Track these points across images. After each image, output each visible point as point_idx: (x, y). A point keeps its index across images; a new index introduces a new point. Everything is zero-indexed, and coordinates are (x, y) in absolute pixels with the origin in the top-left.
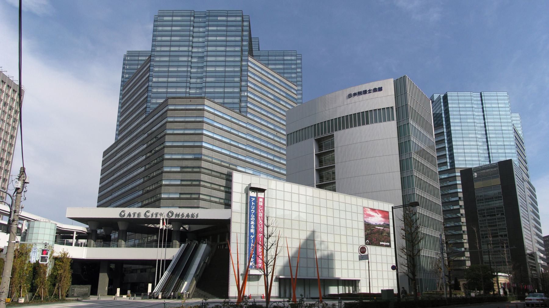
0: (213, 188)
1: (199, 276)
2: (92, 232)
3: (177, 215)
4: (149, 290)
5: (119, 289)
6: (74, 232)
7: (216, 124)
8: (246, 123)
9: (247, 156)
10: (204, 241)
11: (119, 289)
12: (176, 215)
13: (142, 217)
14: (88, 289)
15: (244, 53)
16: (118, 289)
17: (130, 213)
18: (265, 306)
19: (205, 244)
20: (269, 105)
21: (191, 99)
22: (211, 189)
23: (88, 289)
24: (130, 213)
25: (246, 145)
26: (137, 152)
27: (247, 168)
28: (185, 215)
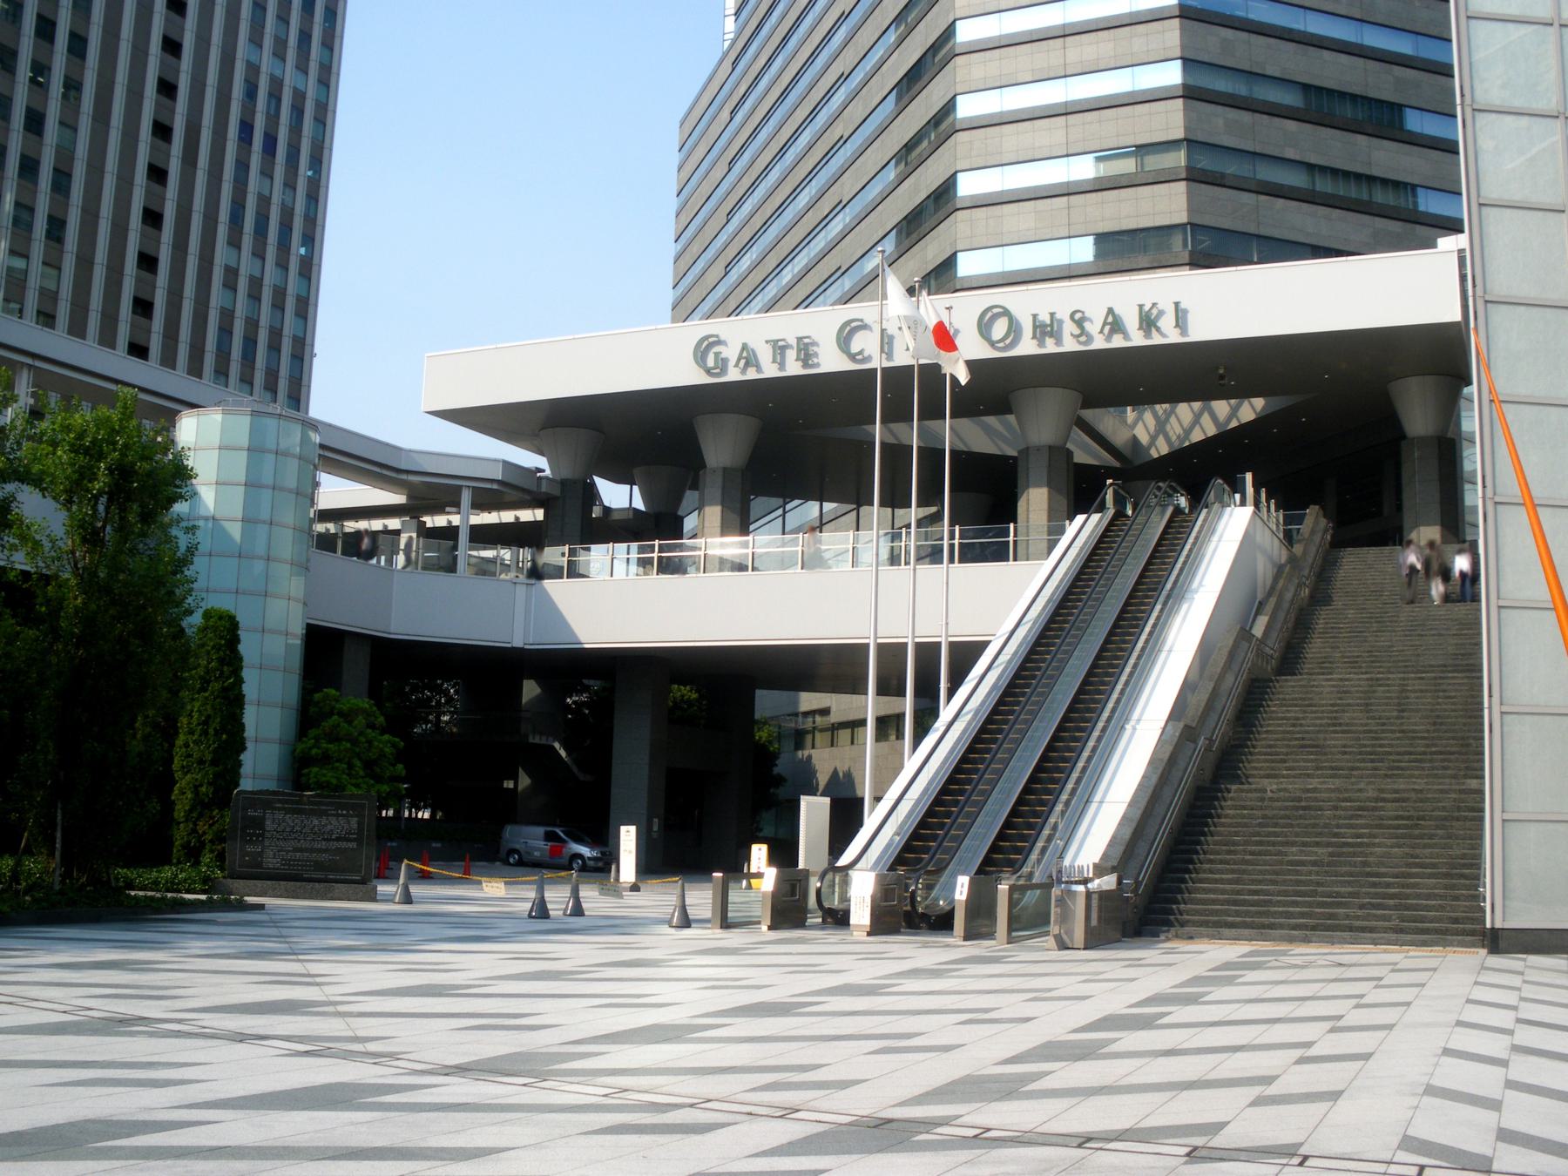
0: (1267, 183)
1: (1201, 741)
2: (563, 491)
3: (1044, 330)
4: (745, 871)
5: (633, 829)
6: (459, 489)
10: (1236, 486)
11: (633, 829)
13: (831, 361)
14: (354, 821)
16: (623, 829)
17: (1110, 311)
19: (1243, 503)
22: (1253, 196)
23: (360, 824)
24: (1110, 311)
26: (941, 1114)
28: (1131, 321)
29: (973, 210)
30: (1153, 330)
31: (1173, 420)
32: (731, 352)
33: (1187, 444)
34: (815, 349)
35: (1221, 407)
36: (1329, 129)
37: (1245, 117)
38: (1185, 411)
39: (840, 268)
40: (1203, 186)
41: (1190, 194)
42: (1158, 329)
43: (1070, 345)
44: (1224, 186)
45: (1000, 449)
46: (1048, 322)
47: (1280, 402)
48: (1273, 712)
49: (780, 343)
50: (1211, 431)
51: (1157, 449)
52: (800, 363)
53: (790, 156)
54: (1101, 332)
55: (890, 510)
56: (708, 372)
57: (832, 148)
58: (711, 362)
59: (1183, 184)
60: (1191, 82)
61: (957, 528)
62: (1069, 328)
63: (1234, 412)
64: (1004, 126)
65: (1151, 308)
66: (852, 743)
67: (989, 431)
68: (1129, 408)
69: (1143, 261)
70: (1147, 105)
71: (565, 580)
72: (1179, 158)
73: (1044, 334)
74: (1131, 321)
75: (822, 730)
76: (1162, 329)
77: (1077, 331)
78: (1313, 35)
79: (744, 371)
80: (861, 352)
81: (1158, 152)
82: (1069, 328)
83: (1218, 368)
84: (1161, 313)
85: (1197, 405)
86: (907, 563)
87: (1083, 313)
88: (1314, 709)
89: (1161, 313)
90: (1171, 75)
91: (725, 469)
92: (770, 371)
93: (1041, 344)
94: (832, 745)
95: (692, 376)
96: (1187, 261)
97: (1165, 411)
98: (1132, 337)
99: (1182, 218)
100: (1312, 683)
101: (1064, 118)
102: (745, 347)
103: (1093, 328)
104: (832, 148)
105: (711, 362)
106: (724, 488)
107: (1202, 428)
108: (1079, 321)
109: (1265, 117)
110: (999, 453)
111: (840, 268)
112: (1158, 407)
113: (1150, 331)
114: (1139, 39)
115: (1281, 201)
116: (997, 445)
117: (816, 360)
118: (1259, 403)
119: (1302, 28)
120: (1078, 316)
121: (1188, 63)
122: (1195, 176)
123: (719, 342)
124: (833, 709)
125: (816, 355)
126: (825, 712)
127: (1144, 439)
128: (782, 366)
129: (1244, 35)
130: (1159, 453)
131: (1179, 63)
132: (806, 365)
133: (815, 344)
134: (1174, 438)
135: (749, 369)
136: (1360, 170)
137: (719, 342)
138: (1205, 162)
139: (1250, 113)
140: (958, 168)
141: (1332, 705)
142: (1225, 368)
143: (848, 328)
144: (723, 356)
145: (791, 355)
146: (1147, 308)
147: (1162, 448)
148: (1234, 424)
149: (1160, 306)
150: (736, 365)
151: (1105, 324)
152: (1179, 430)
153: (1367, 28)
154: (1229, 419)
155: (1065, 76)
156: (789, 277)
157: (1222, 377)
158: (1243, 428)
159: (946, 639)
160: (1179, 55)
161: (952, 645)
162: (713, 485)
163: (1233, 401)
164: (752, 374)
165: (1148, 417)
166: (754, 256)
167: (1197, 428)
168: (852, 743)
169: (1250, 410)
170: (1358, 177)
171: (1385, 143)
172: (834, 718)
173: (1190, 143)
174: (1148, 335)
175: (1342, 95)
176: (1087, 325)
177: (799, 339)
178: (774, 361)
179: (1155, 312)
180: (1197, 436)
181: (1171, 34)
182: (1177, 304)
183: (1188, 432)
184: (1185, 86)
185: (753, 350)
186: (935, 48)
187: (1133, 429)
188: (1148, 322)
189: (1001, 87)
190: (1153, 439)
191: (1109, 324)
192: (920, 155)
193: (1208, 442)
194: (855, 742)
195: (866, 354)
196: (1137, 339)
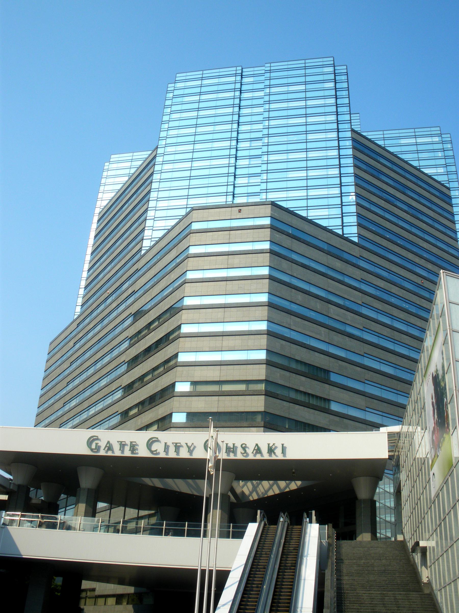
3: (231, 450)
7: (295, 257)
8: (359, 257)
9: (365, 355)
12: (229, 450)
13: (143, 452)
15: (346, 219)
17: (257, 445)
18: (398, 536)
20: (401, 223)
21: (240, 208)
24: (257, 445)
25: (361, 303)
27: (367, 409)
28: (265, 450)
29: (181, 397)
30: (273, 453)
31: (260, 486)
32: (103, 444)
33: (266, 496)
34: (137, 447)
35: (282, 484)
36: (316, 381)
37: (287, 374)
38: (266, 484)
39: (118, 411)
40: (271, 398)
41: (265, 400)
42: (275, 453)
43: (239, 456)
44: (278, 399)
45: (191, 491)
46: (232, 447)
47: (307, 483)
48: (347, 606)
49: (123, 443)
50: (277, 492)
51: (252, 497)
52: (130, 452)
53: (99, 365)
54: (253, 453)
55: (137, 510)
56: (92, 450)
57: (119, 365)
58: (93, 446)
59: (264, 396)
60: (269, 359)
61: (231, 524)
62: (240, 450)
63: (287, 486)
64: (196, 367)
65: (273, 446)
66: (105, 604)
67: (189, 485)
68: (241, 481)
69: (245, 424)
70: (252, 365)
71: (163, 536)
72: (262, 387)
73: (230, 451)
74: (265, 450)
75: (90, 598)
76: (276, 454)
77: (243, 452)
78: (312, 346)
79: (107, 452)
80: (156, 451)
81: (254, 383)
82: (240, 450)
83: (292, 469)
84: (276, 448)
85: (271, 482)
86: (205, 536)
87: (246, 445)
88: (364, 605)
89: (276, 448)
90: (262, 355)
91: (88, 489)
92: (117, 453)
93: (228, 455)
94: (95, 604)
95: (84, 451)
96: (263, 426)
97: (257, 483)
98: (264, 456)
99: (262, 409)
100: (359, 595)
101: (219, 366)
102: (108, 442)
103: (250, 451)
104: (119, 365)
105: (93, 446)
106: (87, 496)
107: (247, 487)
108: (244, 447)
109: (294, 374)
110: (191, 493)
111: (118, 411)
112: (254, 481)
113: (272, 454)
114: (251, 340)
115: (298, 406)
116: (191, 491)
117: (137, 452)
118: (299, 483)
119: (308, 343)
120: (244, 446)
121: (269, 352)
122: (268, 394)
123: (98, 439)
124: (97, 589)
125: (137, 449)
126: (94, 590)
127: (247, 492)
128: (123, 452)
129: (289, 344)
130: (253, 498)
131: (265, 351)
132: (132, 453)
133: (137, 445)
134: (260, 493)
135: (109, 451)
136: (325, 397)
137: (98, 439)
138: (272, 389)
139: (289, 372)
140: (176, 380)
141: (370, 604)
142: (295, 470)
143: (151, 441)
144: (99, 445)
145: (127, 448)
146: (271, 445)
147: (255, 497)
148: (287, 490)
149: (276, 445)
150: (104, 449)
151: (254, 449)
152: (263, 490)
153: (330, 346)
154: (285, 488)
155: (222, 351)
156: (68, 408)
157: (294, 473)
158: (291, 492)
159: (215, 568)
160: (266, 348)
161: (218, 571)
162: (83, 496)
163: (287, 482)
164: (110, 454)
165: (249, 484)
166: (77, 402)
167: (271, 490)
168: (105, 604)
169: (294, 485)
170: (321, 398)
171: (335, 388)
172: (97, 593)
173: (266, 381)
174: (270, 455)
175: (321, 369)
176: (247, 449)
177: (131, 442)
178: (120, 450)
179: (274, 447)
180: (271, 493)
181: (263, 340)
182: (283, 445)
183: (267, 492)
184: (267, 360)
185: (111, 444)
186: (167, 335)
187: (242, 488)
188: (271, 450)
189: (196, 352)
190: (251, 493)
191: (256, 450)
192: (160, 373)
193: (275, 496)
194: (106, 604)
195: (158, 452)
196: (266, 456)
